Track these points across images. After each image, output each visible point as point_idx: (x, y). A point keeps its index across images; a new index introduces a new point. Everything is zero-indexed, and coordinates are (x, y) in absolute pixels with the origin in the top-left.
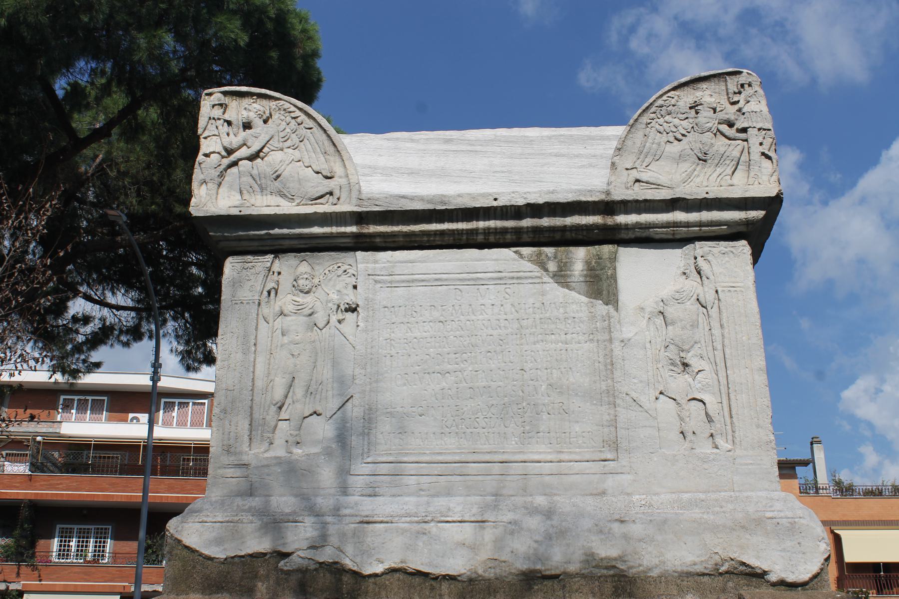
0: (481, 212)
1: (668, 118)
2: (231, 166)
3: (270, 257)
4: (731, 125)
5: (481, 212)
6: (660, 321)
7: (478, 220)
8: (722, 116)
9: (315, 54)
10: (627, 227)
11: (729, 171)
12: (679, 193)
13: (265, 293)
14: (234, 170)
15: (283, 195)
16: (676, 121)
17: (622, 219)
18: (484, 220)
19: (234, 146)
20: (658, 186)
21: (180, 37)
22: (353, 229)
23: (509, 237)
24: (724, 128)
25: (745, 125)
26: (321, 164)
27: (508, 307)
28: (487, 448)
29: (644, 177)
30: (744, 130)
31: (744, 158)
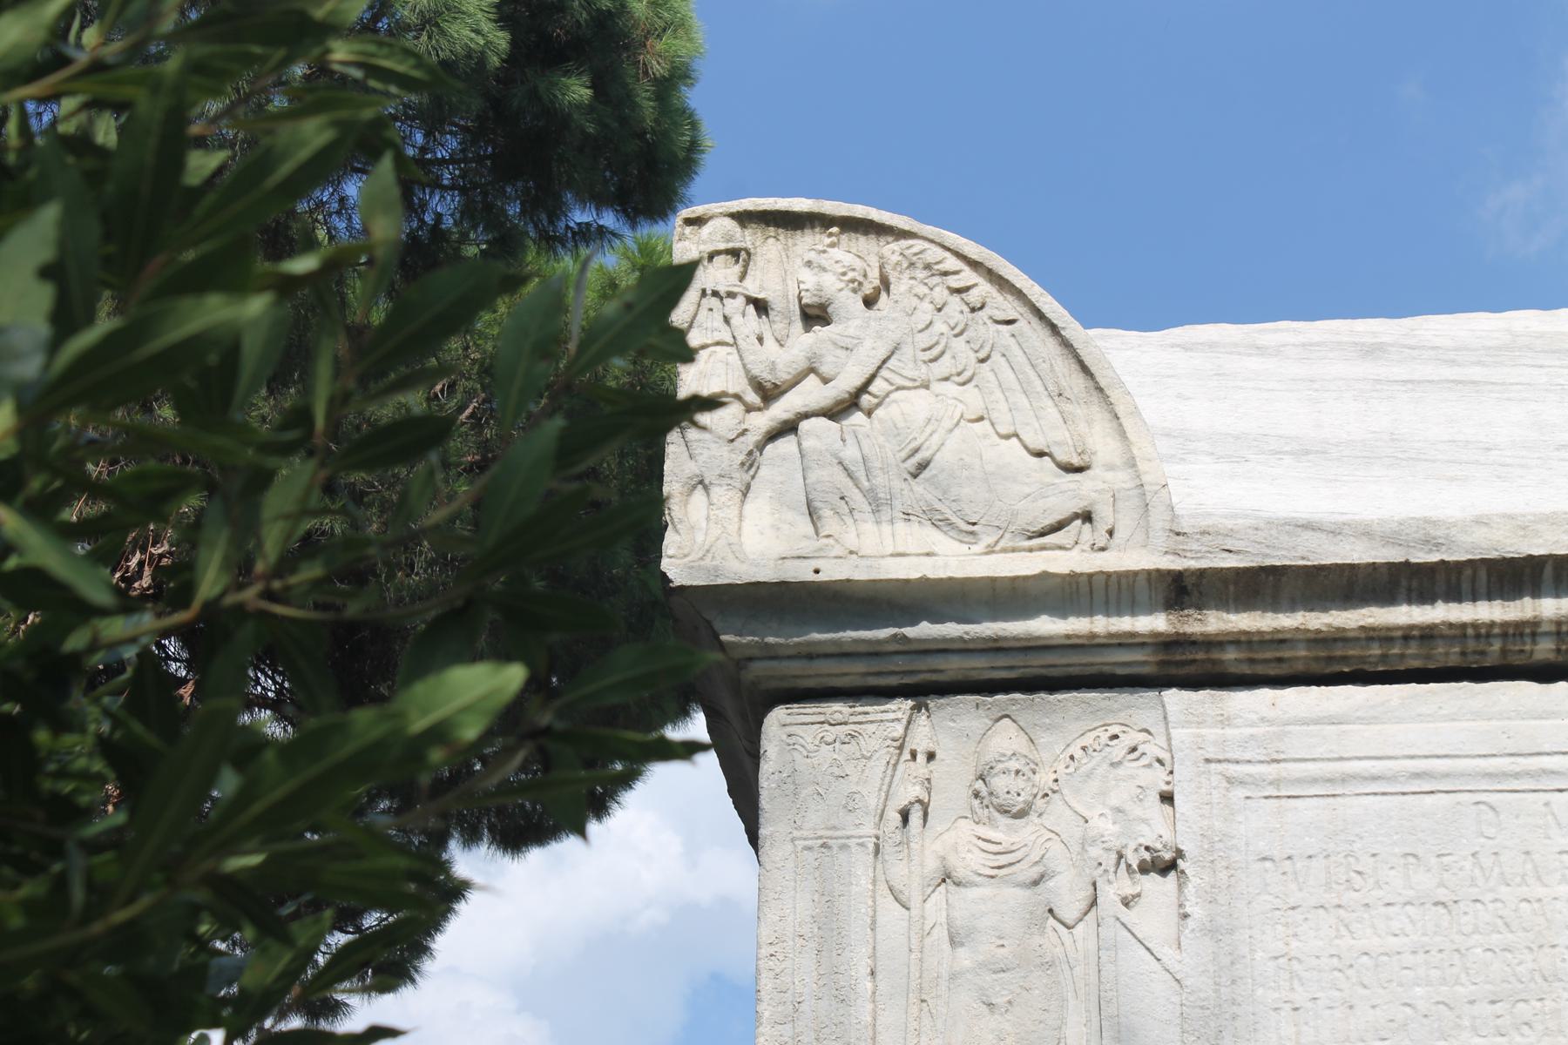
0: (1548, 571)
5: (1548, 571)
7: (1536, 593)
14: (786, 445)
18: (1557, 596)
22: (1156, 623)
23: (1230, 655)
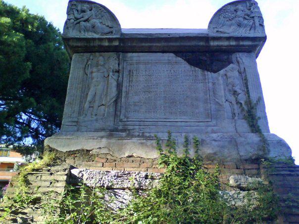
1: (227, 13)
2: (77, 24)
3: (89, 54)
4: (248, 16)
6: (225, 77)
8: (246, 13)
9: (28, 10)
10: (243, 46)
11: (249, 29)
12: (232, 35)
13: (87, 66)
14: (78, 25)
15: (95, 33)
16: (230, 15)
17: (241, 43)
19: (79, 18)
20: (225, 33)
21: (229, 180)
22: (166, 44)
24: (247, 17)
25: (253, 15)
26: (110, 24)
27: (172, 71)
28: (165, 117)
29: (220, 30)
30: (253, 17)
31: (253, 26)
